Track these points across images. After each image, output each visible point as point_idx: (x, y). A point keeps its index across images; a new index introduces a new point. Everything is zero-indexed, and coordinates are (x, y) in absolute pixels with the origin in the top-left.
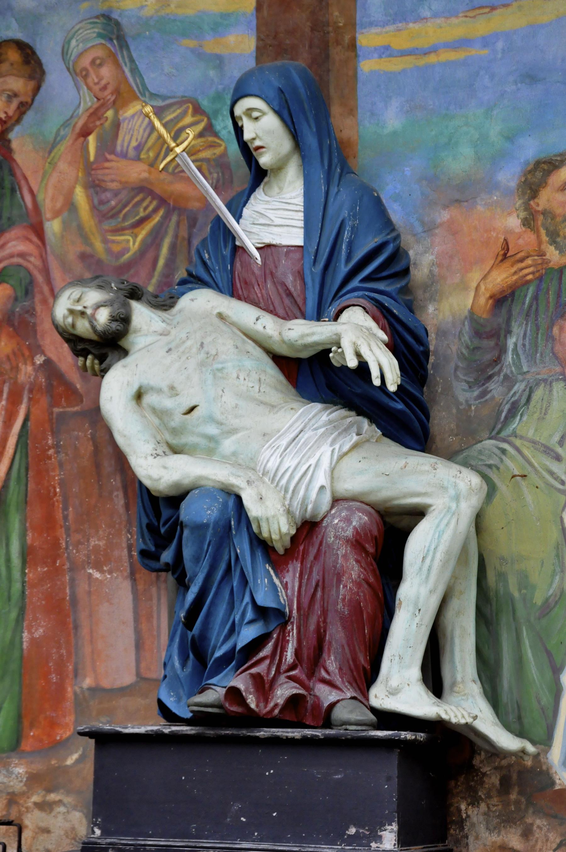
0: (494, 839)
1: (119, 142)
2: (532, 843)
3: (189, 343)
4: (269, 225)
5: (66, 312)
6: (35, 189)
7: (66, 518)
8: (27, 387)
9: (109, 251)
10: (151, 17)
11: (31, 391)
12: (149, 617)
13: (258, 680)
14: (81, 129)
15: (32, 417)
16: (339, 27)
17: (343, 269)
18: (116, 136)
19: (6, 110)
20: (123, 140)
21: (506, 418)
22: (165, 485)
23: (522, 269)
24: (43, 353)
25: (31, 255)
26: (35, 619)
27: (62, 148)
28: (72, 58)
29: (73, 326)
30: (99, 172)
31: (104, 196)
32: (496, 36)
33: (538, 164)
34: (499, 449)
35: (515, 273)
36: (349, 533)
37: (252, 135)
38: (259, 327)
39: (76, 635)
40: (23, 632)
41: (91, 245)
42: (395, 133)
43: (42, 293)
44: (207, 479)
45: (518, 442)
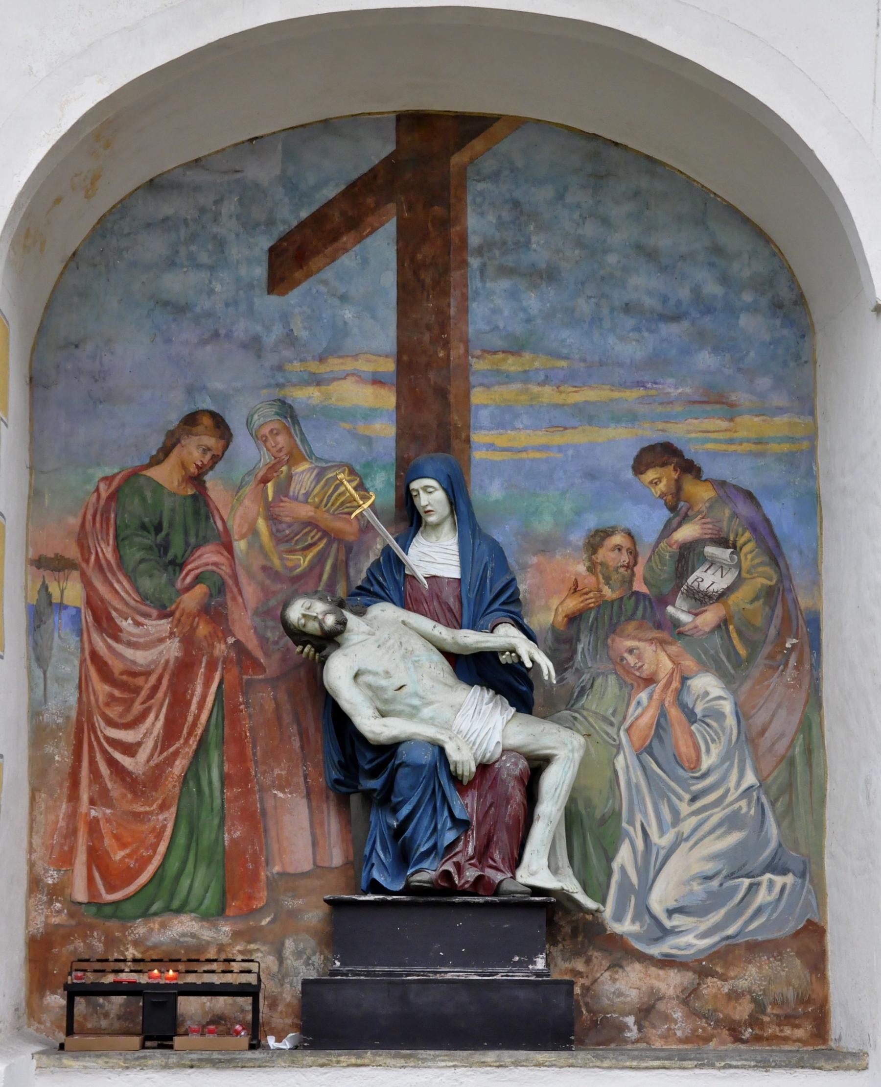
0: (567, 966)
2: (591, 967)
3: (391, 642)
4: (433, 562)
5: (300, 616)
6: (225, 518)
7: (254, 754)
8: (221, 659)
9: (285, 567)
10: (317, 405)
11: (224, 662)
12: (322, 824)
13: (458, 866)
14: (262, 478)
15: (225, 681)
16: (458, 427)
17: (489, 597)
18: (289, 485)
19: (202, 459)
20: (295, 488)
21: (577, 696)
22: (385, 737)
23: (586, 600)
24: (233, 635)
25: (223, 564)
26: (233, 825)
27: (247, 490)
28: (255, 427)
30: (276, 509)
31: (280, 527)
33: (597, 532)
34: (573, 717)
35: (582, 602)
36: (517, 772)
37: (426, 503)
38: (436, 632)
39: (266, 837)
40: (224, 834)
41: (270, 560)
42: (497, 501)
43: (232, 592)
44: (419, 735)
45: (585, 713)
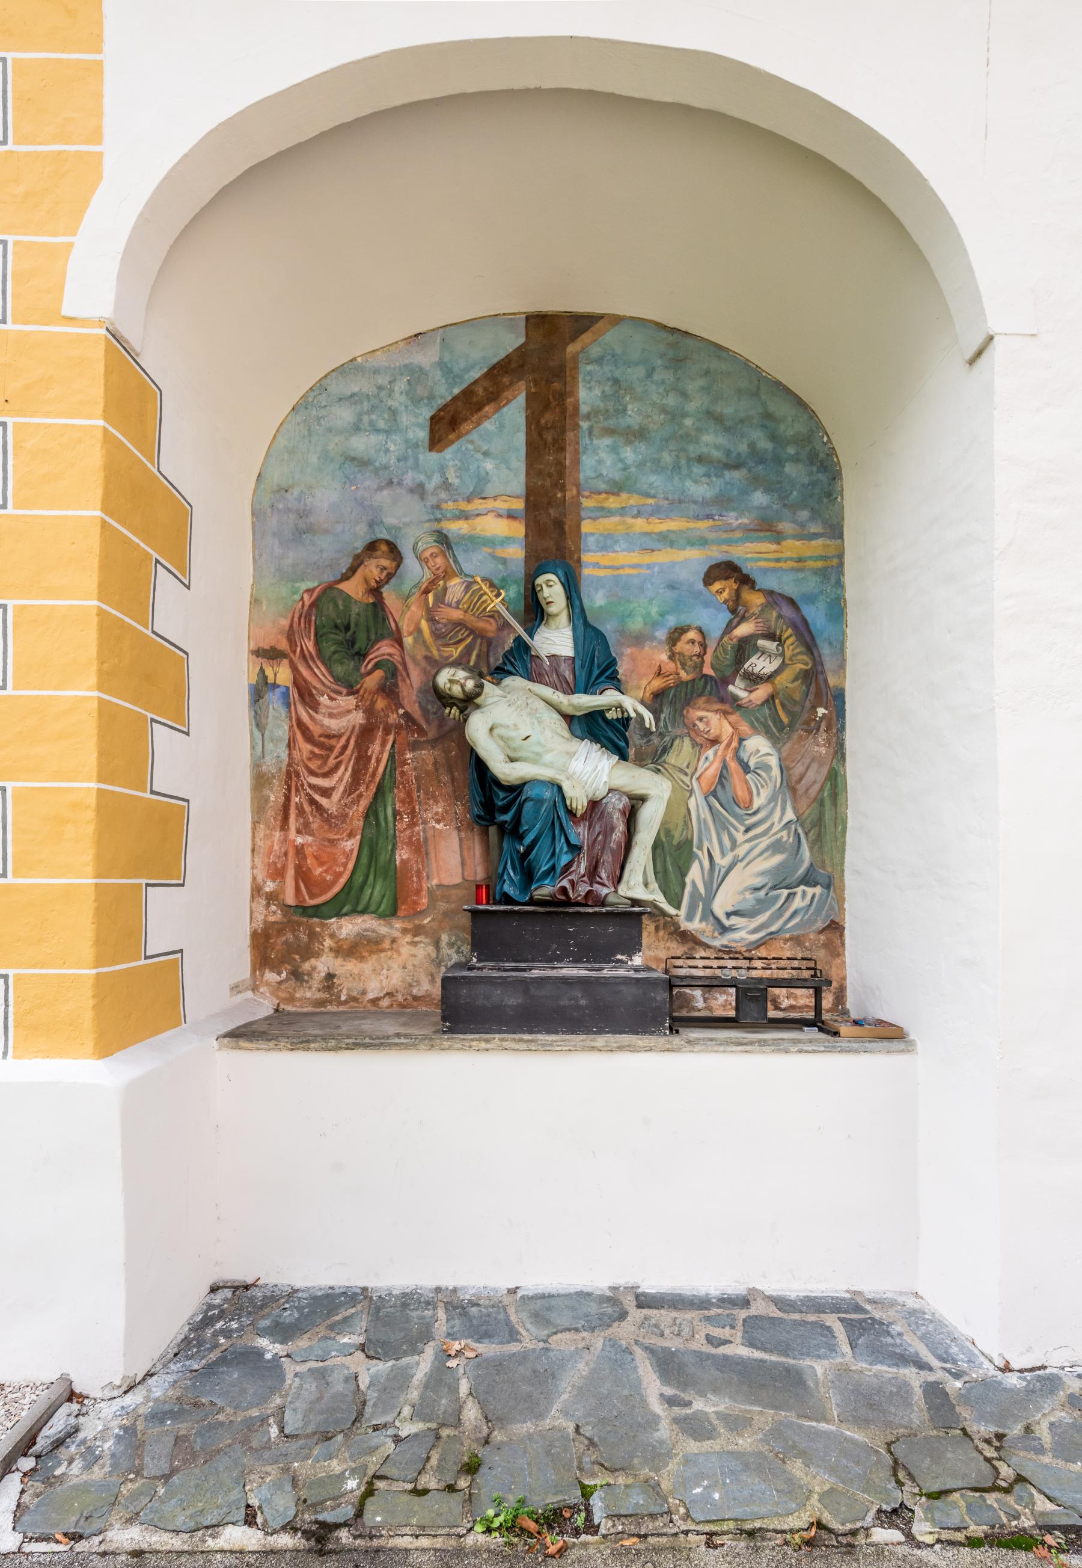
1: (447, 598)
9: (441, 656)
13: (572, 882)
17: (596, 672)
29: (450, 689)
32: (654, 564)
33: (676, 629)
36: (621, 806)
41: (431, 652)
42: (601, 607)
45: (666, 766)
